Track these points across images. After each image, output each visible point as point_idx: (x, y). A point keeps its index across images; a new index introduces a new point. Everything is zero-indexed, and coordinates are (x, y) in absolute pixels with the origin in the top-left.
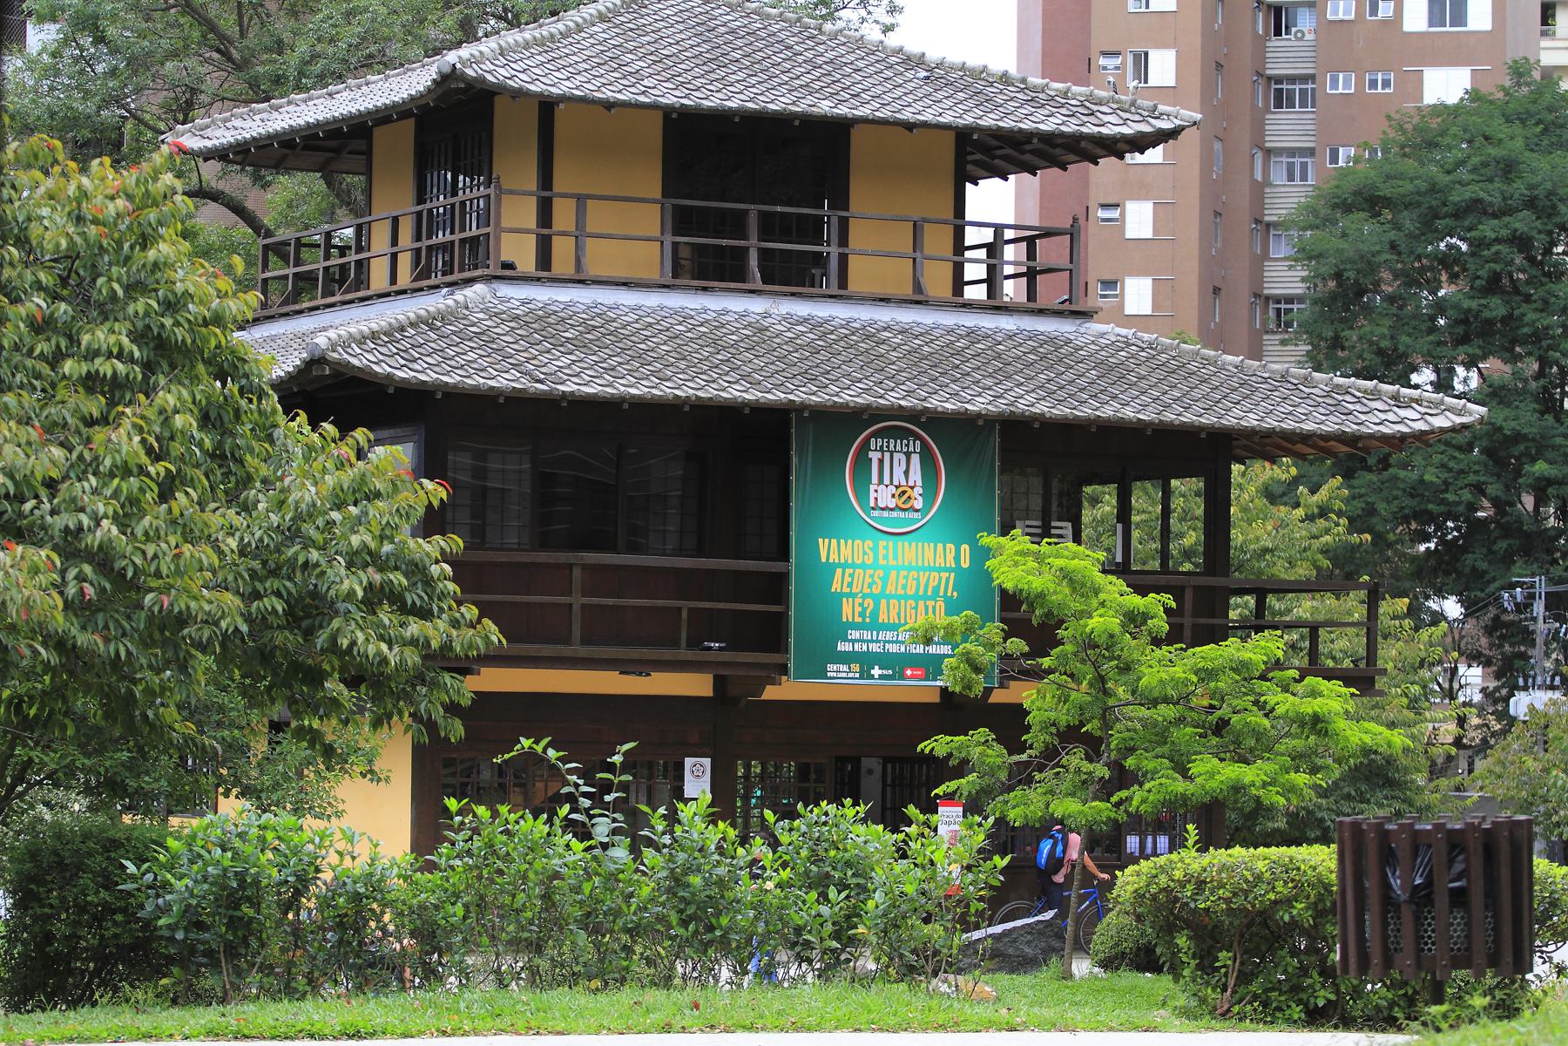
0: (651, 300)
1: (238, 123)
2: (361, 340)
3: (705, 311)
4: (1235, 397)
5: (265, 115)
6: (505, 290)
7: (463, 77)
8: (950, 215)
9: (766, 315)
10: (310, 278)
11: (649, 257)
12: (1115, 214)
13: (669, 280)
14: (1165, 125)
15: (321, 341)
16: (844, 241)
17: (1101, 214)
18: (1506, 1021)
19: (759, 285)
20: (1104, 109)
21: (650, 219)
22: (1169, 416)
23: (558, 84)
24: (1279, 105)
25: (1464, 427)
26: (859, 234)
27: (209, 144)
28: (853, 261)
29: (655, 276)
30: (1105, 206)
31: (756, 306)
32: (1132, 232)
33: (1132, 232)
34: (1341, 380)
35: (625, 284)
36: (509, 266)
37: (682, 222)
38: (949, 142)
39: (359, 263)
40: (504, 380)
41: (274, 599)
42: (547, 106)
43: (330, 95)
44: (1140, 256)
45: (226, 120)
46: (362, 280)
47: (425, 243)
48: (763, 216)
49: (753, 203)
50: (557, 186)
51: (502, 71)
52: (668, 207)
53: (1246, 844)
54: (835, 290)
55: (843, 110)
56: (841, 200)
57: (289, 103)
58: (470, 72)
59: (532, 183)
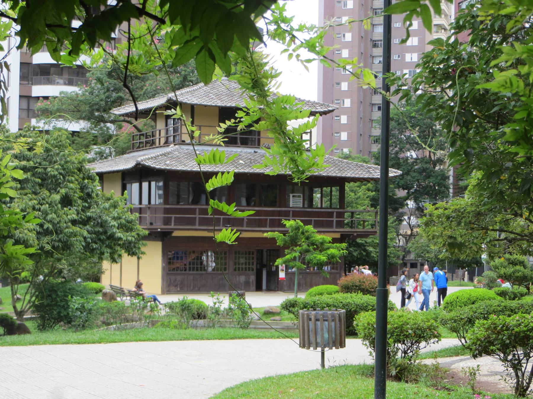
1: (127, 108)
2: (149, 159)
3: (228, 151)
4: (346, 169)
9: (241, 152)
10: (142, 143)
12: (338, 118)
14: (330, 109)
15: (139, 159)
17: (336, 118)
18: (267, 376)
19: (239, 145)
22: (330, 174)
24: (375, 94)
25: (397, 176)
27: (120, 113)
28: (261, 139)
30: (336, 116)
31: (239, 150)
32: (342, 122)
33: (342, 122)
34: (369, 165)
36: (184, 141)
39: (152, 140)
40: (180, 168)
44: (344, 127)
46: (153, 143)
53: (316, 286)
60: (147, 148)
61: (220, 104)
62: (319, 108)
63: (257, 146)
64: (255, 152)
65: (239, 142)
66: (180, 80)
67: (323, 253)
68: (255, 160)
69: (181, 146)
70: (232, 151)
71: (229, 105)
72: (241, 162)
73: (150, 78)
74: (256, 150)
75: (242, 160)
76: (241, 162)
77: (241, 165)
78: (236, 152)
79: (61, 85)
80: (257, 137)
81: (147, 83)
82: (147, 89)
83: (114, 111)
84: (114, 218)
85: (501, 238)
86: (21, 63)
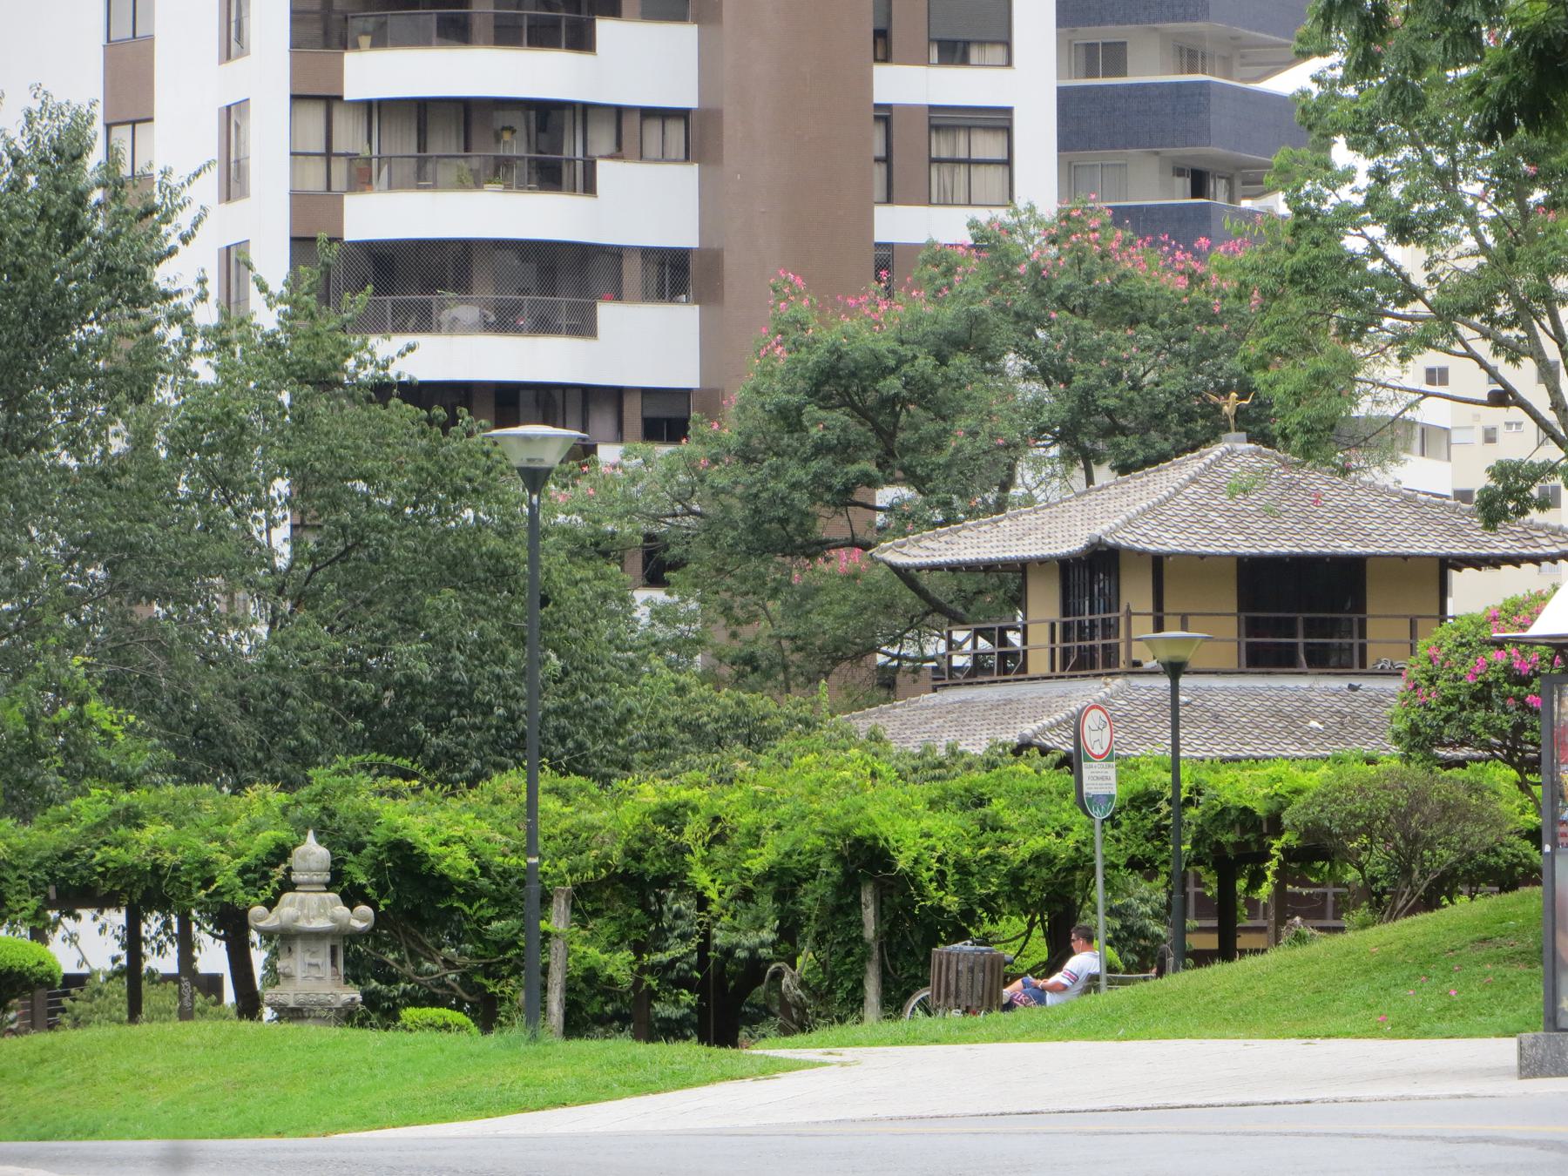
0: (1234, 682)
2: (1051, 728)
5: (946, 538)
6: (1137, 681)
7: (1105, 544)
8: (1436, 613)
9: (1311, 689)
11: (1229, 653)
13: (1244, 668)
16: (1363, 634)
19: (1305, 668)
20: (1540, 534)
21: (1229, 627)
23: (1168, 541)
26: (1372, 627)
28: (1370, 648)
29: (1234, 666)
31: (1303, 683)
35: (1215, 673)
36: (1137, 664)
37: (1252, 627)
38: (1437, 563)
41: (105, 848)
42: (1158, 562)
43: (995, 522)
45: (917, 541)
47: (1075, 644)
48: (1308, 622)
49: (1300, 611)
50: (1166, 609)
51: (1131, 537)
52: (1243, 616)
54: (1356, 669)
55: (1358, 550)
56: (1360, 607)
57: (964, 528)
58: (1110, 540)
59: (1148, 606)
60: (1011, 677)
61: (1245, 549)
62: (1545, 541)
63: (1356, 669)
64: (1353, 688)
65: (1302, 657)
66: (1068, 405)
67: (38, 818)
68: (1355, 717)
69: (1130, 678)
70: (1283, 689)
71: (1270, 549)
72: (1314, 724)
73: (968, 406)
74: (1356, 682)
75: (1315, 717)
76: (1314, 724)
77: (1315, 734)
78: (1297, 689)
79: (469, 330)
80: (1356, 641)
81: (963, 423)
82: (958, 450)
83: (885, 550)
84: (1143, 900)
85: (542, 798)
86: (293, 239)
